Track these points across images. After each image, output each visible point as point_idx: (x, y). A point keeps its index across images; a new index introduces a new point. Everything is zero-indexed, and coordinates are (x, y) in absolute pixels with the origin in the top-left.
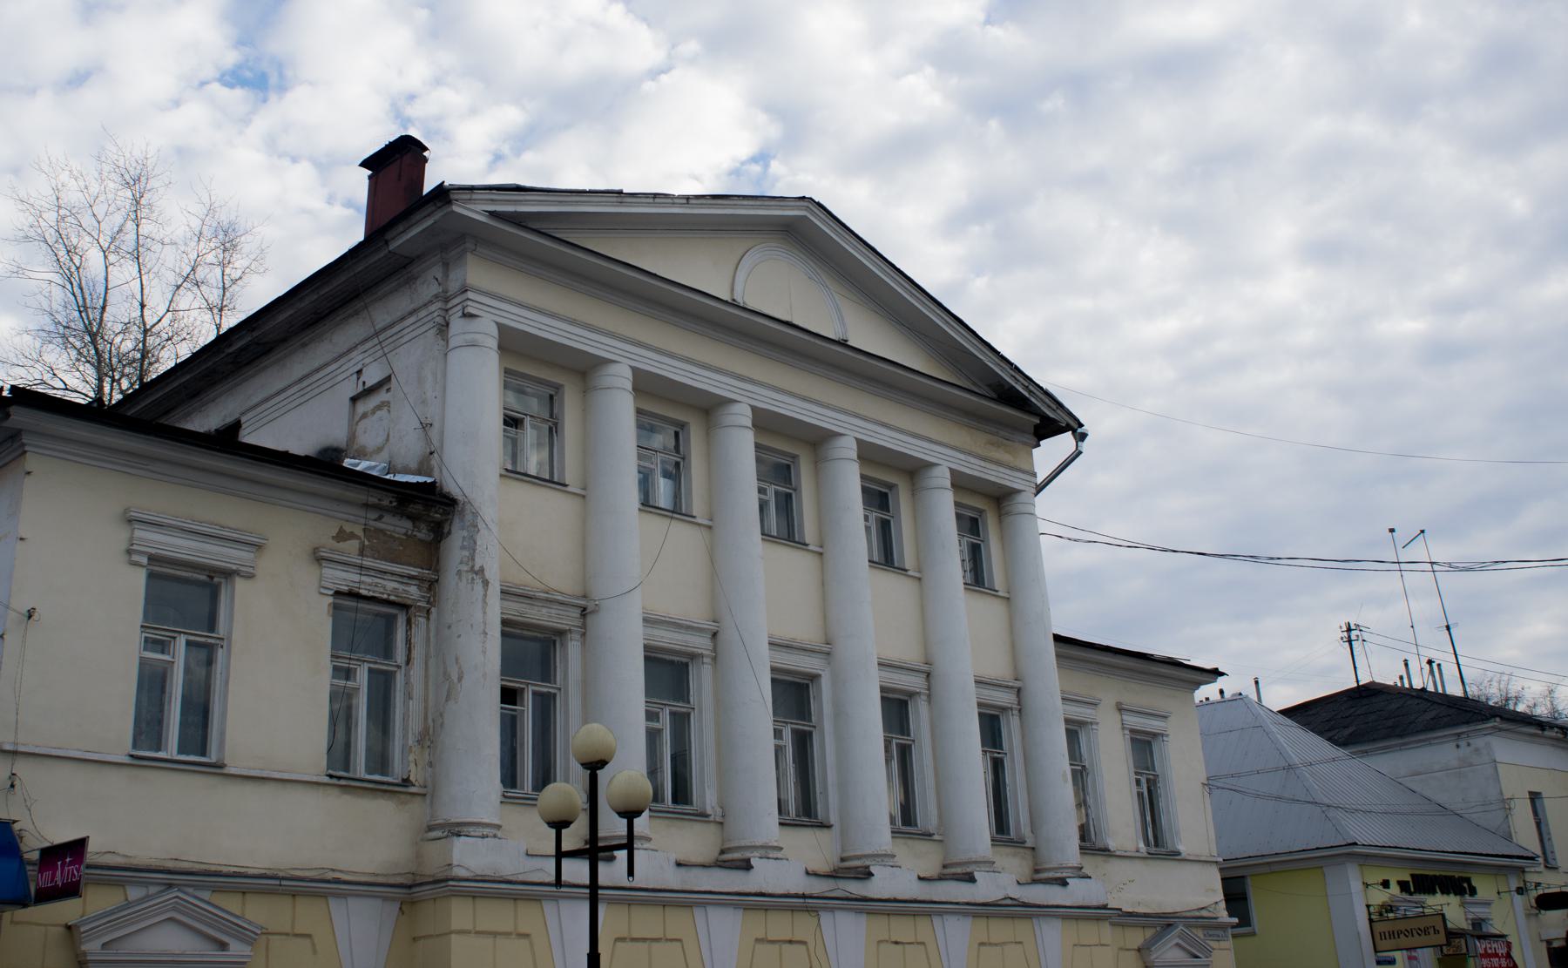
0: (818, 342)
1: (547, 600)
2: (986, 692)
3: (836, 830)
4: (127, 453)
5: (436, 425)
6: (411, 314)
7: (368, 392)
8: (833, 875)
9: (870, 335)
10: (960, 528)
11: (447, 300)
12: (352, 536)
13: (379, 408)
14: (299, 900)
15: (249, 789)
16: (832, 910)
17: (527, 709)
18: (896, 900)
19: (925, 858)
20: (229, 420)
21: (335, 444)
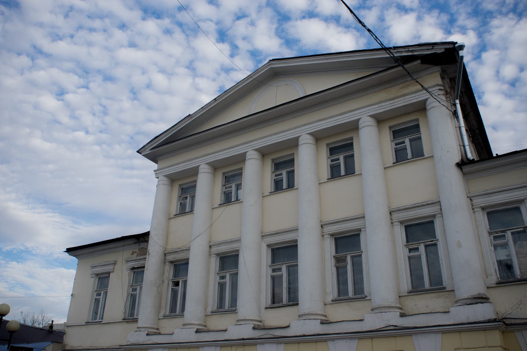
0: (270, 111)
1: (181, 251)
2: (94, 270)
4: (89, 253)
12: (136, 252)
14: (374, 340)
15: (107, 326)
16: (263, 343)
17: (228, 279)
18: (304, 336)
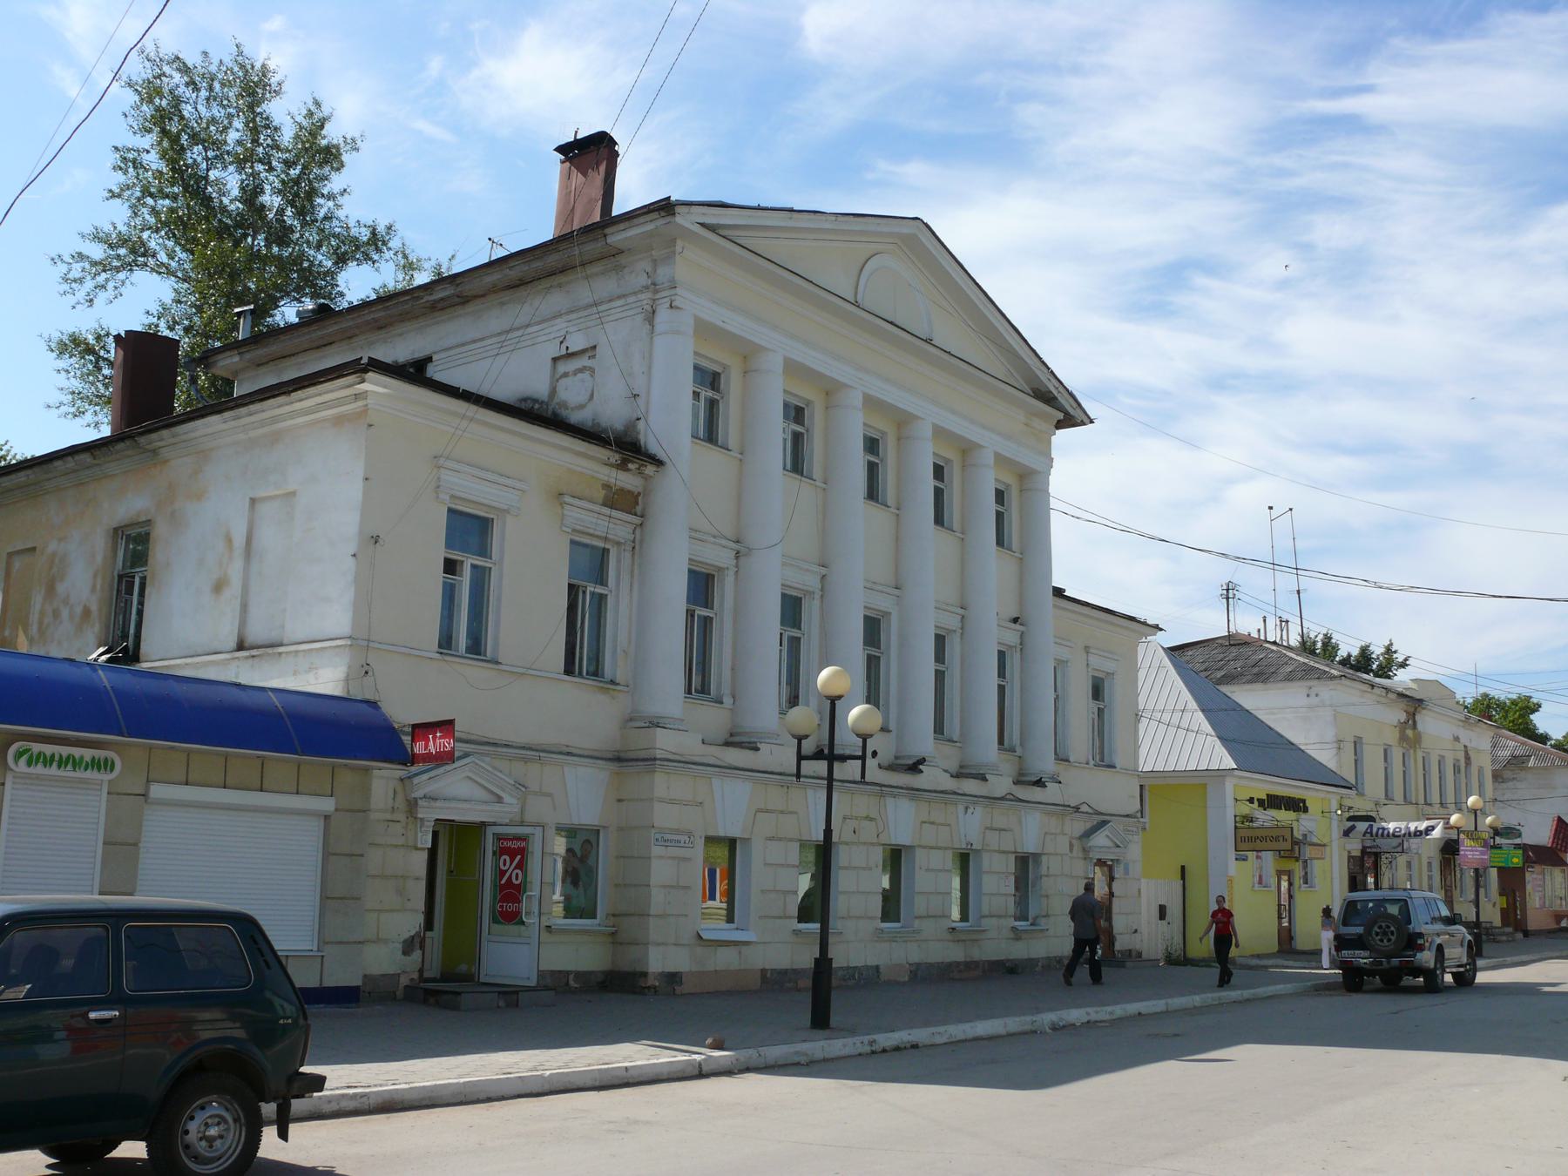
3: (893, 734)
5: (643, 395)
6: (619, 297)
7: (570, 355)
8: (958, 776)
9: (952, 334)
10: (786, 417)
11: (656, 292)
13: (581, 370)
19: (711, 718)
20: (419, 355)
21: (536, 396)
